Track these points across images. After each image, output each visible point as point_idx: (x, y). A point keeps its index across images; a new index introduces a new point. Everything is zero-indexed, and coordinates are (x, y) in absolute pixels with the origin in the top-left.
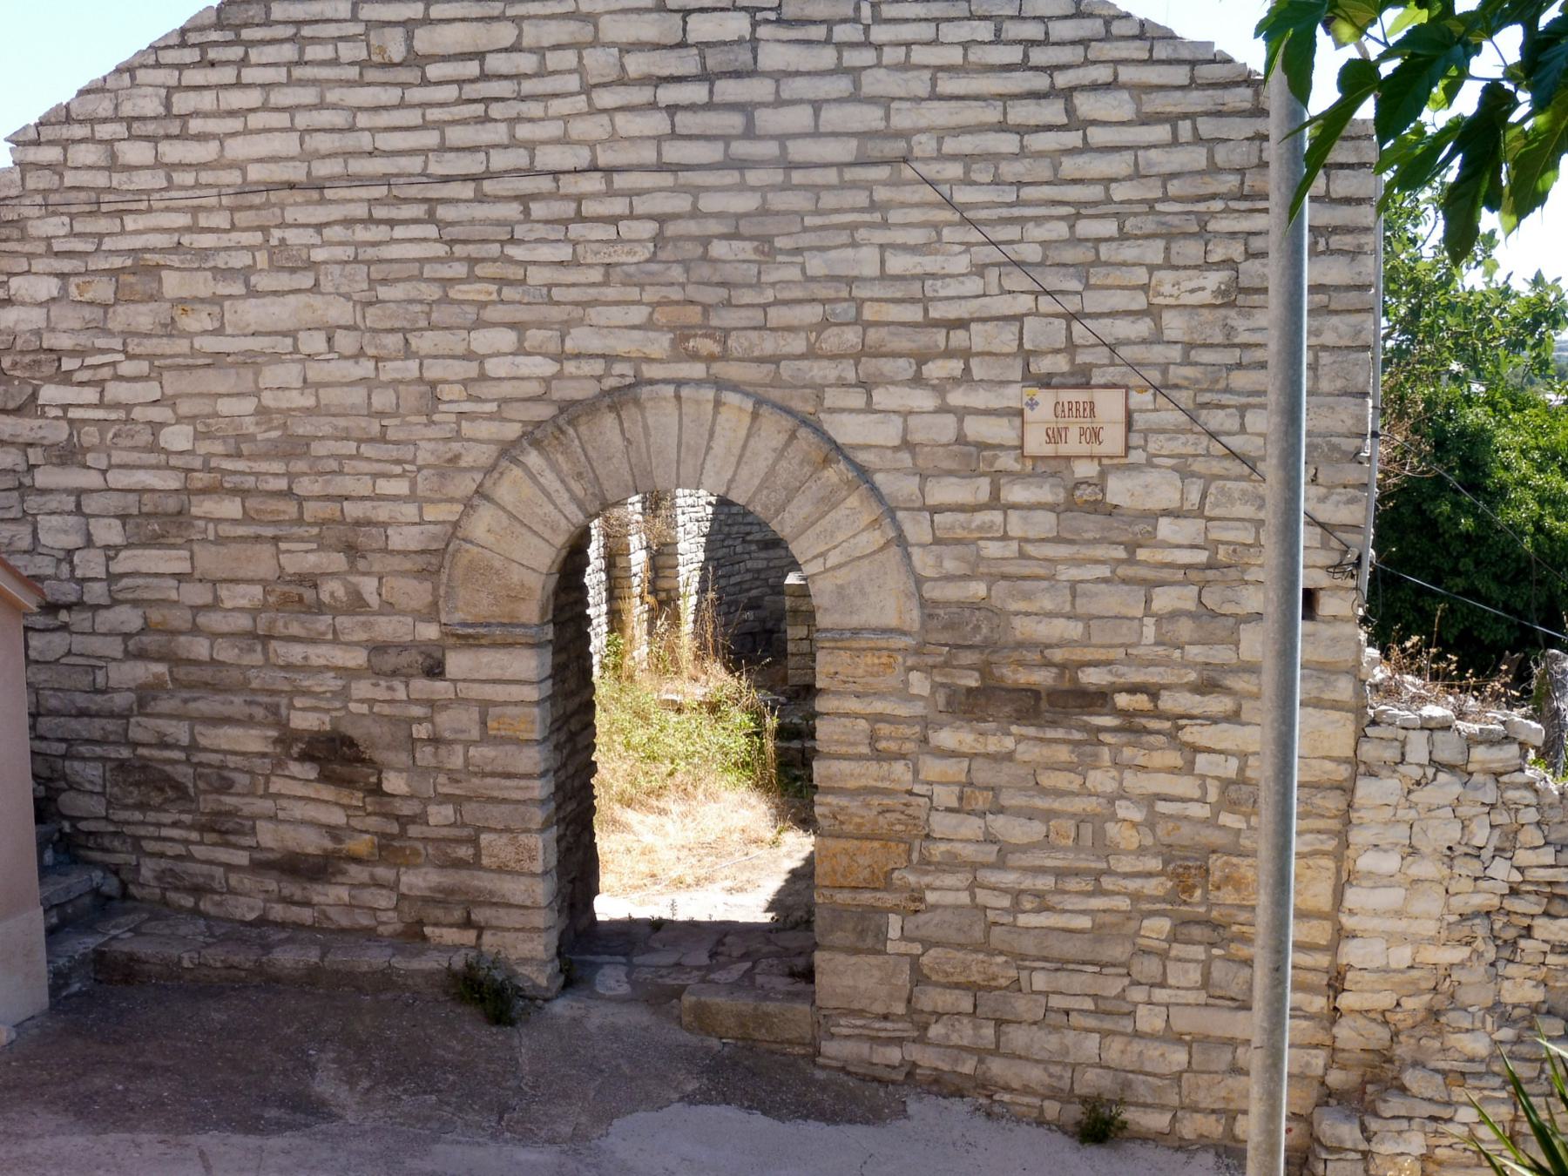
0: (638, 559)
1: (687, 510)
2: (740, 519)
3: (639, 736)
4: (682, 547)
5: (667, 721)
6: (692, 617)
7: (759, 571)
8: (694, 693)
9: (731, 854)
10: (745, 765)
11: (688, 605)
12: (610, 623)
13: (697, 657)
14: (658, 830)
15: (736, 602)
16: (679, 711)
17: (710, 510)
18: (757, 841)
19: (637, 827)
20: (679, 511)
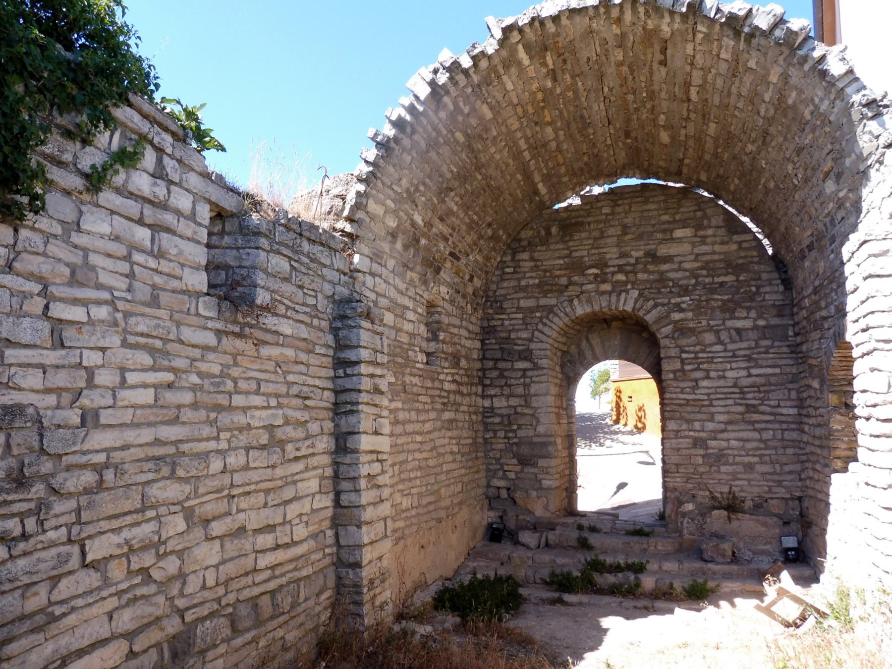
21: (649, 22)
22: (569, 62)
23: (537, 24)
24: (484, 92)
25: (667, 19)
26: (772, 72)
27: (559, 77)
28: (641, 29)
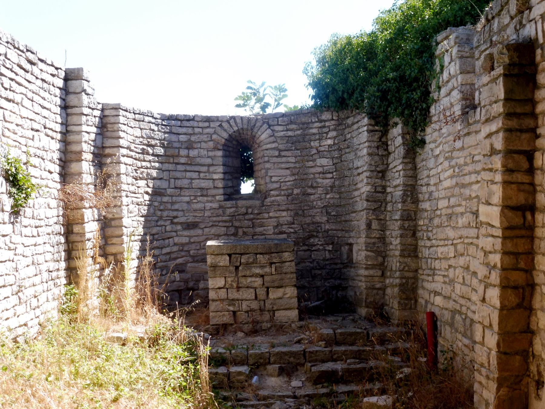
2: (169, 206)
4: (126, 221)
6: (134, 276)
7: (183, 245)
10: (182, 389)
12: (68, 277)
15: (166, 267)
17: (147, 197)
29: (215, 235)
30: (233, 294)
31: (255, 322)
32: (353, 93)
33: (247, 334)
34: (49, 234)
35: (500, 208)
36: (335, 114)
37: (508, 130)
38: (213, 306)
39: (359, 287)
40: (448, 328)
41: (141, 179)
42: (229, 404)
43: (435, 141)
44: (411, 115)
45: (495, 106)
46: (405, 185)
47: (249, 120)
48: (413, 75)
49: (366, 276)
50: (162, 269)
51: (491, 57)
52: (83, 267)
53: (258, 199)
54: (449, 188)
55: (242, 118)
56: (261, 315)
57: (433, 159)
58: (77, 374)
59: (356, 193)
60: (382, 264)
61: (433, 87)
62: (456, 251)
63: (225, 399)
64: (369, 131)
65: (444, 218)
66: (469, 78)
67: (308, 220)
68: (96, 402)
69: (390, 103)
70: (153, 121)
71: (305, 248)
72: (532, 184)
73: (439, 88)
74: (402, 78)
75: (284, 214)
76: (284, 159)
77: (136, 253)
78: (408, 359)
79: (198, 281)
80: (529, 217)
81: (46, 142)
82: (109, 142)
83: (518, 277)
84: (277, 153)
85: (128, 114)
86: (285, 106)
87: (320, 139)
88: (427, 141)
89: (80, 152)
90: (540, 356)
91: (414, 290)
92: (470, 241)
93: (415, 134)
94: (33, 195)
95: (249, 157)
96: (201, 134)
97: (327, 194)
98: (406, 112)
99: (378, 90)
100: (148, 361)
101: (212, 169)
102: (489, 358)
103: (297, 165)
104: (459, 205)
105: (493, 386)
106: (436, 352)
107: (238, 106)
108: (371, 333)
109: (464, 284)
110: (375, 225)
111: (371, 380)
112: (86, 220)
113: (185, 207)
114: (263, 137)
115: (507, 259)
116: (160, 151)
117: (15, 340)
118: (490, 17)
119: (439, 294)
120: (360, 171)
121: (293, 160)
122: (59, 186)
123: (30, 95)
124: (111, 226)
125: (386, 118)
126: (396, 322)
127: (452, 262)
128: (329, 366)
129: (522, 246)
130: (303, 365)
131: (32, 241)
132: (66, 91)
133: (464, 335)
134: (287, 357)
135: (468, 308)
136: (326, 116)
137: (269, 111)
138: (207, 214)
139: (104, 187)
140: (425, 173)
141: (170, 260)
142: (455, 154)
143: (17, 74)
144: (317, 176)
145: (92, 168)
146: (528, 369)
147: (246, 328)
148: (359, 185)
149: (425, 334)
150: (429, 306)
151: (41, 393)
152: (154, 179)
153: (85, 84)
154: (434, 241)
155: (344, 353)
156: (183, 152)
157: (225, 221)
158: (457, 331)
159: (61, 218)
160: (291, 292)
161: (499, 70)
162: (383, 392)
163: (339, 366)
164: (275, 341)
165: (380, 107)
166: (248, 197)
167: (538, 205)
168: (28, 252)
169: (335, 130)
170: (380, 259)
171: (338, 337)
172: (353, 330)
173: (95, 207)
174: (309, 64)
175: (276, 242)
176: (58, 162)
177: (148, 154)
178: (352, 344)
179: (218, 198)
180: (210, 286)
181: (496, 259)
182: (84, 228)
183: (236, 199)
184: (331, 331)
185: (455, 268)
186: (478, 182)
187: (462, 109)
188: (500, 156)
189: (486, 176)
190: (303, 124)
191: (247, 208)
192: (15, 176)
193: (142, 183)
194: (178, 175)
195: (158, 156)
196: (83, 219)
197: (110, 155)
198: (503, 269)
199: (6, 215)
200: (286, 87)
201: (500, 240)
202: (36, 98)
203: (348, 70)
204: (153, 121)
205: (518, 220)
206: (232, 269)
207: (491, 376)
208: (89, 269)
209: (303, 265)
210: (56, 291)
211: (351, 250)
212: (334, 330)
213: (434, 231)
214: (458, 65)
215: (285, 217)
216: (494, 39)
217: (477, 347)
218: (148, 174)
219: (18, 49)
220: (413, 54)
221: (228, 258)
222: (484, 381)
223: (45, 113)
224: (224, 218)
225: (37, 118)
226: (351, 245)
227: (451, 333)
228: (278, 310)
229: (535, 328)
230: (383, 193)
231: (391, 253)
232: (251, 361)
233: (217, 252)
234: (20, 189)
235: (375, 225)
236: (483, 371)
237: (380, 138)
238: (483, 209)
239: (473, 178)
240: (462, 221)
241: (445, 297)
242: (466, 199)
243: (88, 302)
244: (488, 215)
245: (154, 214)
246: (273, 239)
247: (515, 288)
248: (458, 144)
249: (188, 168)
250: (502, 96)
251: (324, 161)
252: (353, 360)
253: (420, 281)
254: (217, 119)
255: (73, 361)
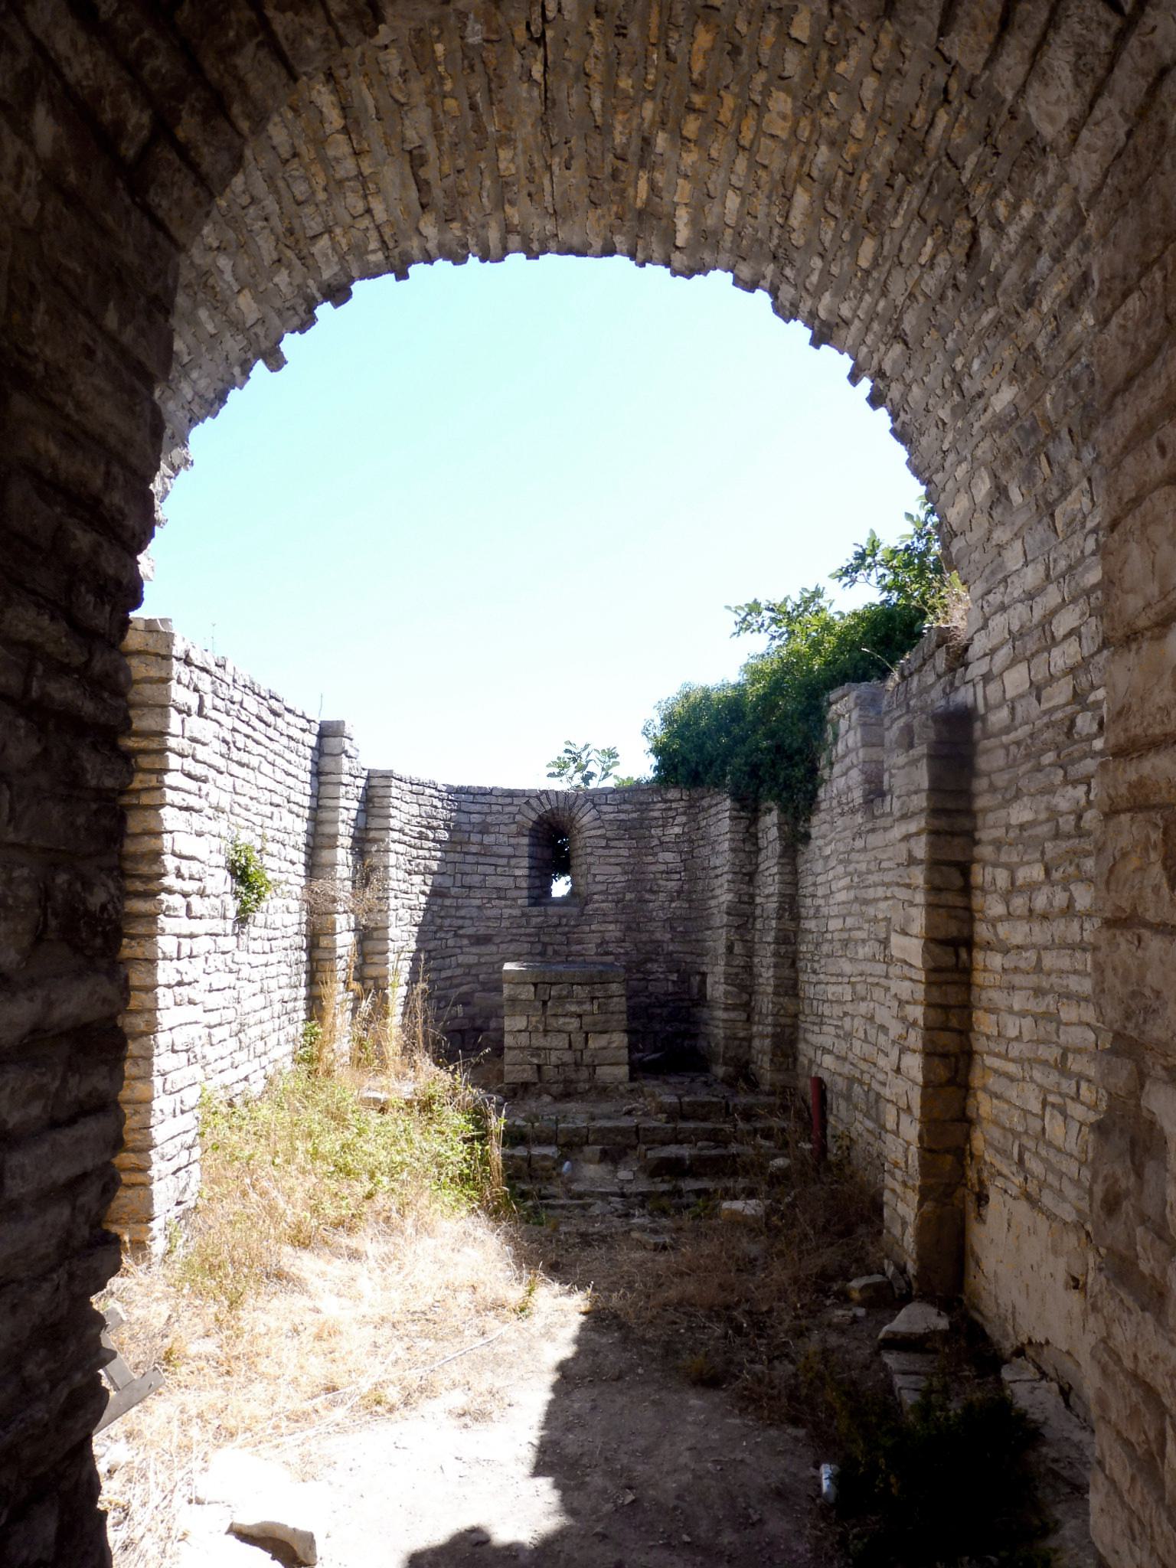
0: (345, 941)
1: (400, 895)
2: (453, 912)
3: (330, 1143)
4: (393, 932)
5: (368, 1123)
6: (401, 1010)
7: (469, 966)
8: (399, 1088)
9: (458, 1332)
11: (397, 994)
13: (404, 1049)
14: (346, 1290)
16: (382, 1111)
17: (423, 899)
18: (498, 1306)
19: (314, 1283)
20: (392, 894)
21: (458, 233)
22: (608, 170)
23: (640, 256)
24: (775, 241)
25: (431, 246)
26: (254, 306)
27: (636, 144)
28: (471, 219)
29: (515, 954)
30: (539, 1041)
31: (568, 1082)
32: (711, 764)
33: (557, 1099)
34: (285, 949)
35: (922, 941)
36: (685, 793)
37: (934, 833)
38: (509, 1056)
39: (715, 1036)
40: (843, 1104)
41: (416, 873)
42: (530, 1203)
43: (824, 837)
44: (791, 799)
45: (914, 797)
46: (781, 895)
47: (566, 795)
48: (795, 745)
49: (725, 1021)
50: (439, 999)
51: (908, 730)
52: (331, 995)
53: (576, 906)
54: (844, 903)
55: (557, 793)
56: (577, 1071)
57: (821, 862)
58: (315, 1155)
59: (713, 903)
60: (747, 1004)
61: (823, 762)
62: (854, 992)
63: (524, 1195)
64: (732, 818)
65: (838, 945)
66: (874, 754)
67: (645, 937)
68: (343, 1198)
69: (762, 782)
70: (436, 794)
71: (640, 976)
72: (968, 909)
73: (831, 764)
74: (779, 748)
75: (612, 927)
76: (613, 852)
77: (405, 976)
78: (786, 1144)
79: (488, 1018)
80: (964, 955)
81: (289, 820)
82: (375, 823)
83: (948, 1041)
84: (603, 843)
85: (402, 784)
86: (616, 777)
87: (664, 826)
88: (813, 836)
89: (335, 836)
90: (982, 1157)
91: (793, 1042)
92: (876, 980)
93: (796, 824)
94: (268, 896)
95: (563, 846)
96: (499, 813)
97: (672, 901)
98: (785, 795)
99: (746, 764)
100: (416, 1137)
101: (513, 862)
102: (906, 1157)
103: (632, 860)
104: (859, 929)
105: (914, 1198)
106: (824, 1136)
107: (551, 775)
108: (731, 1104)
109: (866, 1040)
110: (738, 949)
111: (734, 1174)
112: (338, 930)
113: (475, 913)
114: (586, 819)
115: (932, 1012)
116: (444, 835)
117: (231, 1105)
118: (906, 673)
119: (830, 1052)
120: (719, 871)
121: (625, 853)
122: (303, 882)
123: (271, 757)
124: (372, 939)
125: (757, 800)
126: (767, 1088)
127: (849, 1008)
128: (672, 1151)
129: (953, 996)
130: (634, 1148)
131: (263, 959)
132: (319, 751)
133: (867, 1115)
134: (612, 1136)
135: (873, 1076)
136: (673, 794)
137: (594, 784)
138: (505, 923)
139: (366, 885)
140: (810, 879)
141: (451, 987)
142: (854, 856)
143: (255, 729)
144: (659, 876)
145: (350, 858)
146: (963, 1175)
147: (556, 1089)
148: (718, 892)
149: (808, 1108)
150: (815, 1069)
151: (265, 1184)
152: (433, 873)
153: (347, 743)
154: (822, 976)
155: (694, 1131)
156: (475, 838)
157: (529, 935)
158: (856, 1108)
159: (304, 926)
160: (620, 1039)
161: (921, 749)
162: (751, 1194)
163: (685, 1151)
164: (597, 1111)
165: (748, 786)
166: (564, 901)
167: (977, 939)
168: (255, 975)
169: (684, 814)
170: (745, 997)
171: (685, 1107)
172: (707, 1099)
173: (352, 911)
174: (650, 722)
175: (600, 968)
176: (303, 848)
177: (427, 839)
178: (705, 1119)
179: (520, 902)
180: (507, 1028)
181: (917, 1012)
182: (334, 941)
183: (545, 905)
184: (674, 1099)
185: (853, 1017)
186: (886, 898)
187: (865, 796)
188: (922, 867)
189: (902, 894)
190: (641, 804)
191: (560, 917)
192: (244, 869)
193: (417, 879)
194: (467, 868)
195: (440, 842)
196: (334, 929)
197: (375, 841)
198: (927, 1028)
199: (229, 924)
200: (618, 751)
201: (923, 987)
202: (279, 761)
203: (705, 734)
204: (436, 794)
205: (948, 959)
206: (539, 1004)
207: (910, 1183)
208: (339, 998)
209: (636, 1000)
210: (291, 1029)
211: (703, 982)
212: (680, 1097)
213: (823, 962)
214: (859, 735)
215: (613, 930)
216: (912, 703)
217: (889, 1138)
218: (426, 867)
219: (259, 695)
220: (796, 716)
221: (532, 989)
222: (899, 1189)
223: (290, 781)
224: (528, 931)
225: (279, 788)
226: (704, 975)
227: (848, 1110)
228: (600, 1065)
229: (974, 1116)
230: (750, 904)
231: (761, 989)
232: (562, 1140)
233: (518, 980)
234: (250, 888)
235: (738, 949)
236: (898, 1173)
237: (747, 828)
238: (896, 939)
239: (880, 892)
240: (863, 951)
241: (838, 1057)
242: (869, 922)
243: (335, 1046)
244: (903, 949)
245: (432, 922)
246: (594, 963)
247: (944, 1056)
248: (859, 844)
249: (481, 860)
250: (925, 785)
251: (669, 856)
252: (705, 1143)
253: (801, 1032)
254: (522, 794)
255: (310, 1135)
